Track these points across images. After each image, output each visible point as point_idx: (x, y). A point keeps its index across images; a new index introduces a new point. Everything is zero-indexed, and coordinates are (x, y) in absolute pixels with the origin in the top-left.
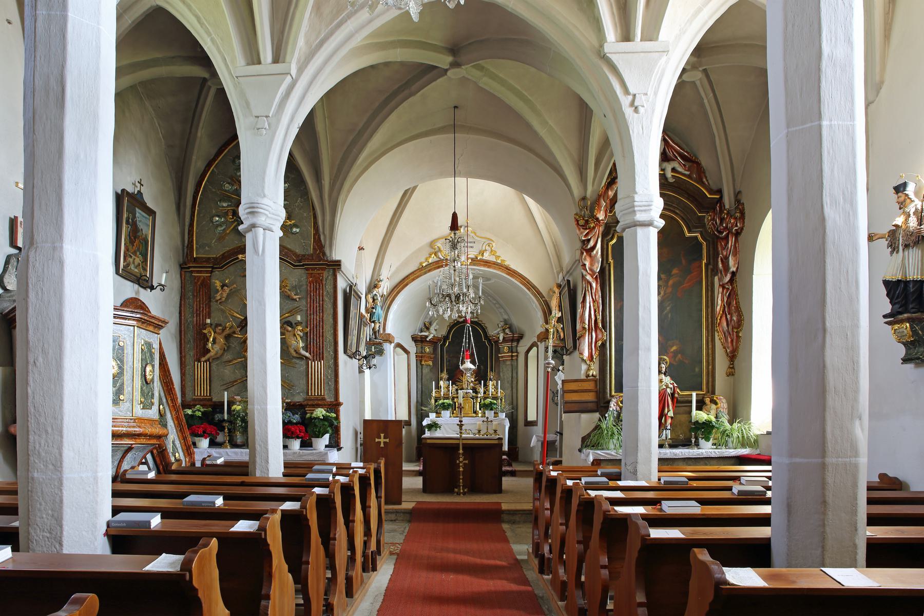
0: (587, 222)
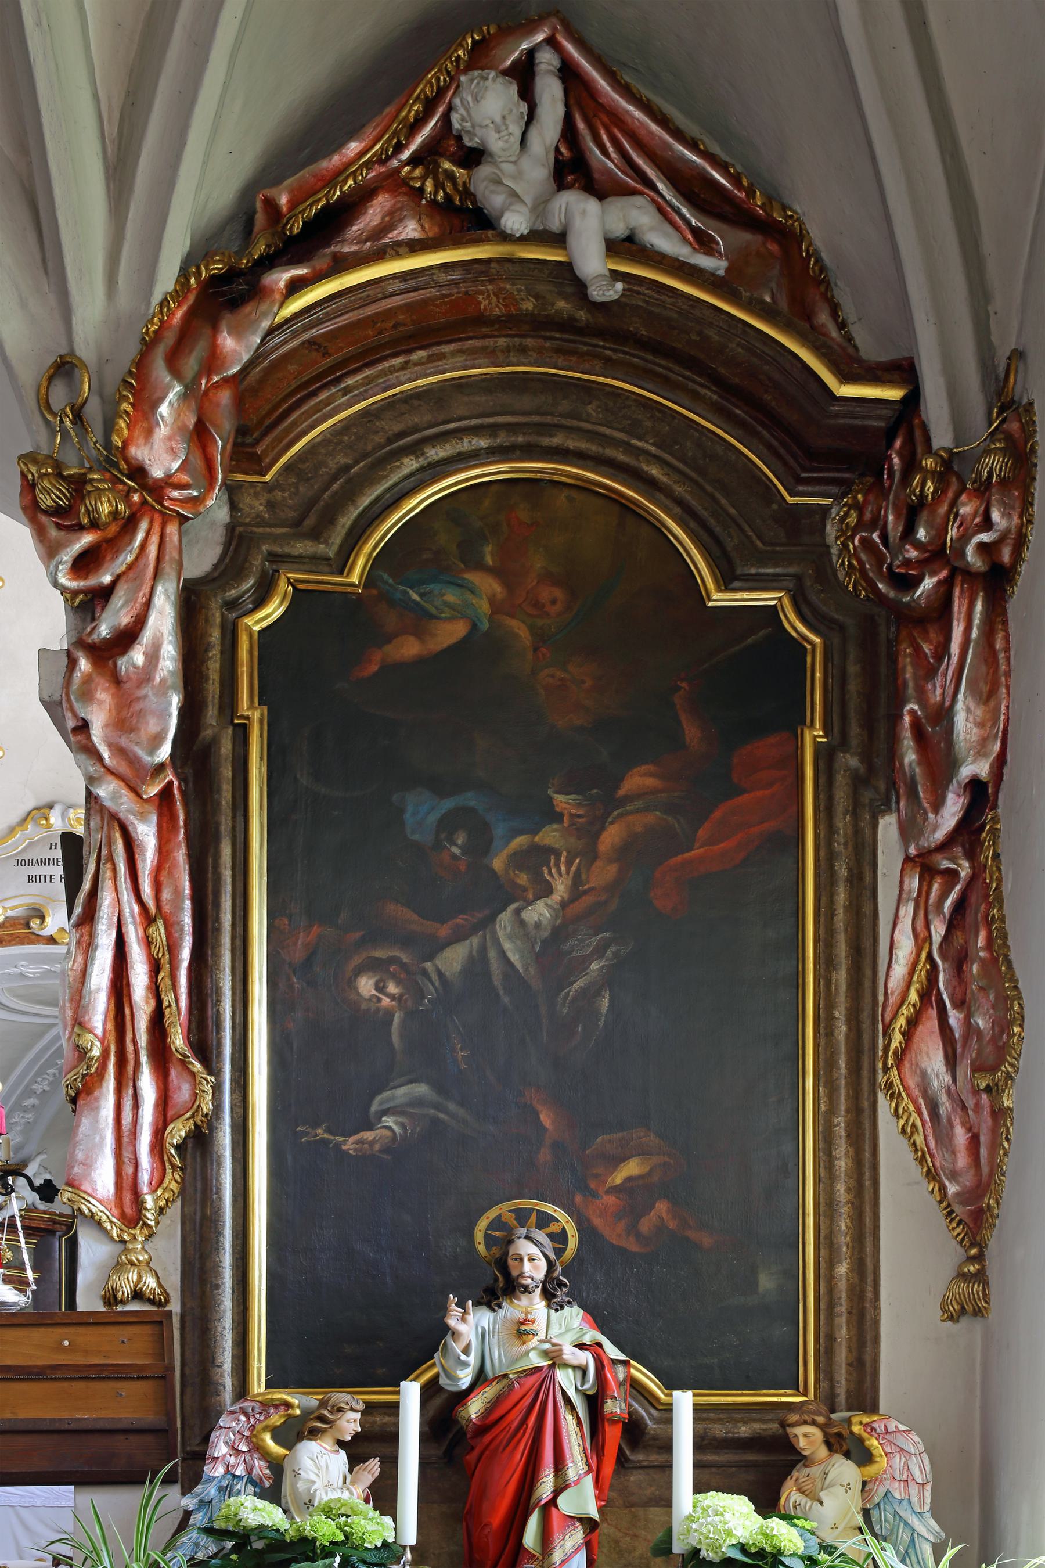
0: (79, 486)
